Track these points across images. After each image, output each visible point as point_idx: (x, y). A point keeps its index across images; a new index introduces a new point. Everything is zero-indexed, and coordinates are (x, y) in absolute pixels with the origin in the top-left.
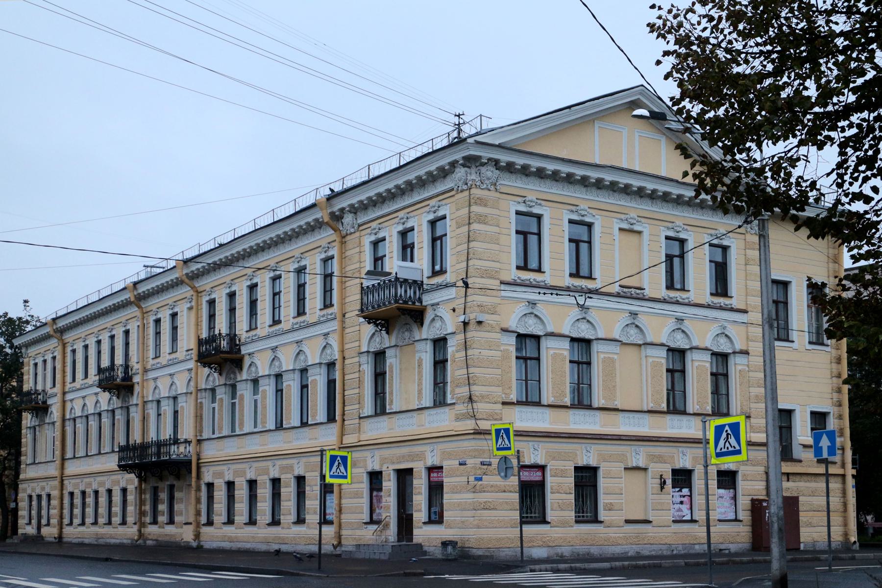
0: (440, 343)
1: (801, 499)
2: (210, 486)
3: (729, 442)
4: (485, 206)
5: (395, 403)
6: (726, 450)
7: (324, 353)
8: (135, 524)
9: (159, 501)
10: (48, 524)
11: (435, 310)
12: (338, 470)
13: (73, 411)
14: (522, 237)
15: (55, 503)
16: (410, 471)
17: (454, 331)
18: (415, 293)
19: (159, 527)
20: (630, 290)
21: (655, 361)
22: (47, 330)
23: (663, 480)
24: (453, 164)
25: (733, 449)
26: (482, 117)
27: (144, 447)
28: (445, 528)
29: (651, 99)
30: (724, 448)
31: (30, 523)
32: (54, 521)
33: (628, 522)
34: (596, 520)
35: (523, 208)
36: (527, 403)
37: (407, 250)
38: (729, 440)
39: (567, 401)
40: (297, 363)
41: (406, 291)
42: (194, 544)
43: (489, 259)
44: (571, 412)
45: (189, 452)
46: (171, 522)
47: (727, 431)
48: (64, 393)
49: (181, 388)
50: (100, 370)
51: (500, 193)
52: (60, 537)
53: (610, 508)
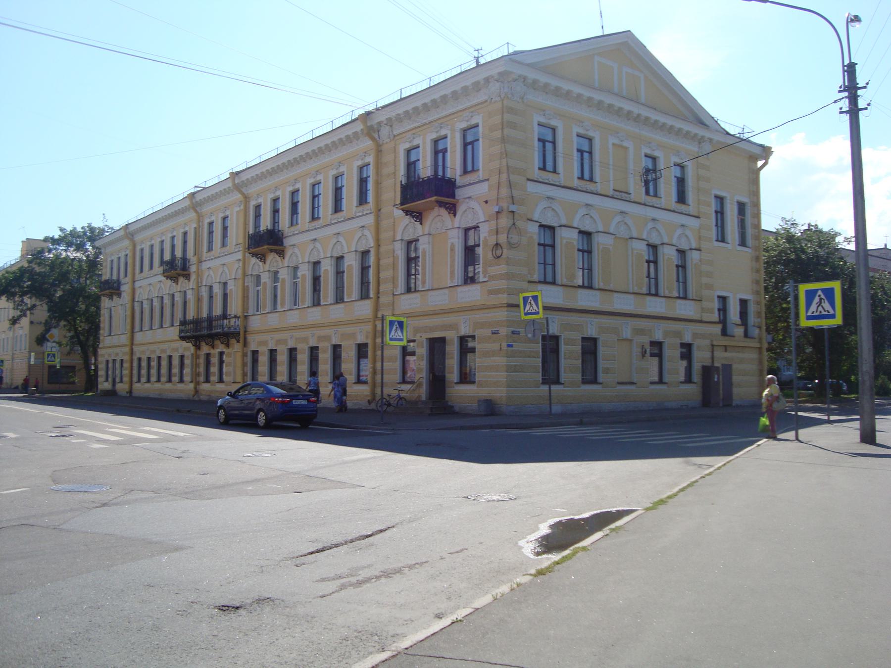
1: (734, 366)
2: (255, 353)
3: (822, 306)
6: (818, 313)
8: (191, 382)
9: (211, 365)
10: (121, 381)
12: (396, 334)
13: (141, 295)
14: (541, 144)
15: (126, 365)
16: (443, 340)
19: (212, 385)
26: (509, 45)
27: (197, 322)
28: (477, 387)
30: (817, 312)
31: (107, 380)
32: (126, 379)
33: (619, 383)
34: (594, 381)
36: (545, 282)
38: (823, 304)
47: (819, 296)
50: (162, 262)
52: (130, 392)
53: (607, 371)
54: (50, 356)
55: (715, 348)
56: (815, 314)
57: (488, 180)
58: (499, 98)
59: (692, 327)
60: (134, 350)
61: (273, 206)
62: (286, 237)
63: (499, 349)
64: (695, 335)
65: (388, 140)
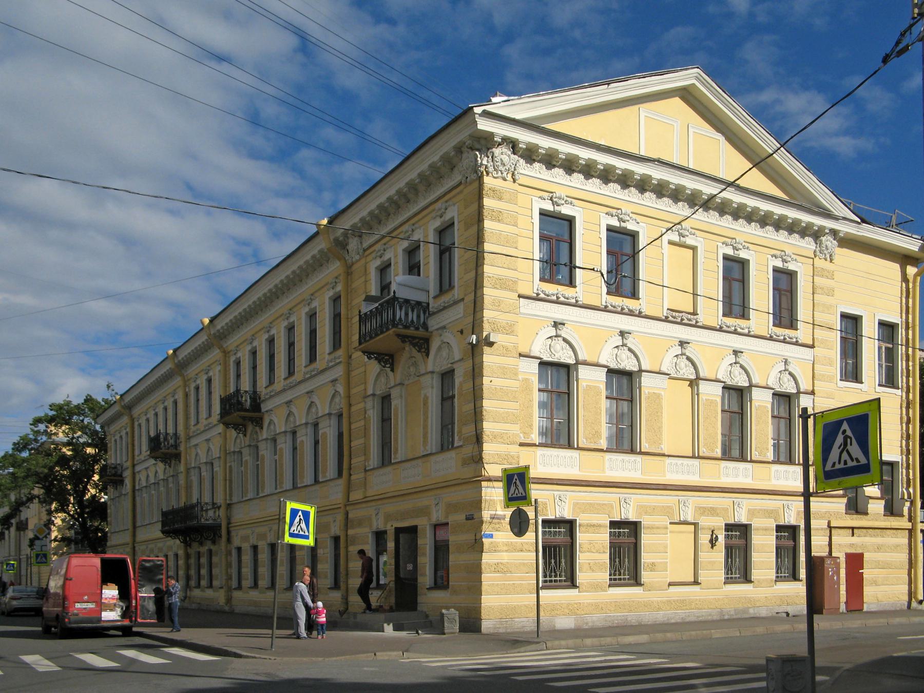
0: (447, 376)
1: (866, 556)
2: (239, 549)
4: (500, 199)
5: (400, 451)
6: (842, 466)
7: (333, 403)
11: (441, 335)
17: (461, 358)
18: (418, 316)
20: (681, 315)
21: (709, 400)
22: (116, 408)
23: (714, 536)
24: (459, 150)
25: (855, 463)
29: (709, 86)
30: (839, 463)
34: (636, 580)
35: (548, 206)
37: (414, 268)
38: (849, 447)
39: (604, 444)
40: (310, 416)
41: (407, 314)
42: (227, 608)
43: (504, 266)
44: (608, 456)
45: (219, 516)
46: (211, 586)
47: (844, 432)
48: (134, 466)
49: (216, 452)
51: (520, 185)
53: (653, 567)
54: (40, 557)
55: (833, 531)
56: (837, 466)
57: (463, 299)
58: (475, 175)
59: (695, 500)
60: (137, 549)
61: (252, 362)
62: (263, 401)
63: (474, 541)
64: (752, 513)
65: (357, 257)
